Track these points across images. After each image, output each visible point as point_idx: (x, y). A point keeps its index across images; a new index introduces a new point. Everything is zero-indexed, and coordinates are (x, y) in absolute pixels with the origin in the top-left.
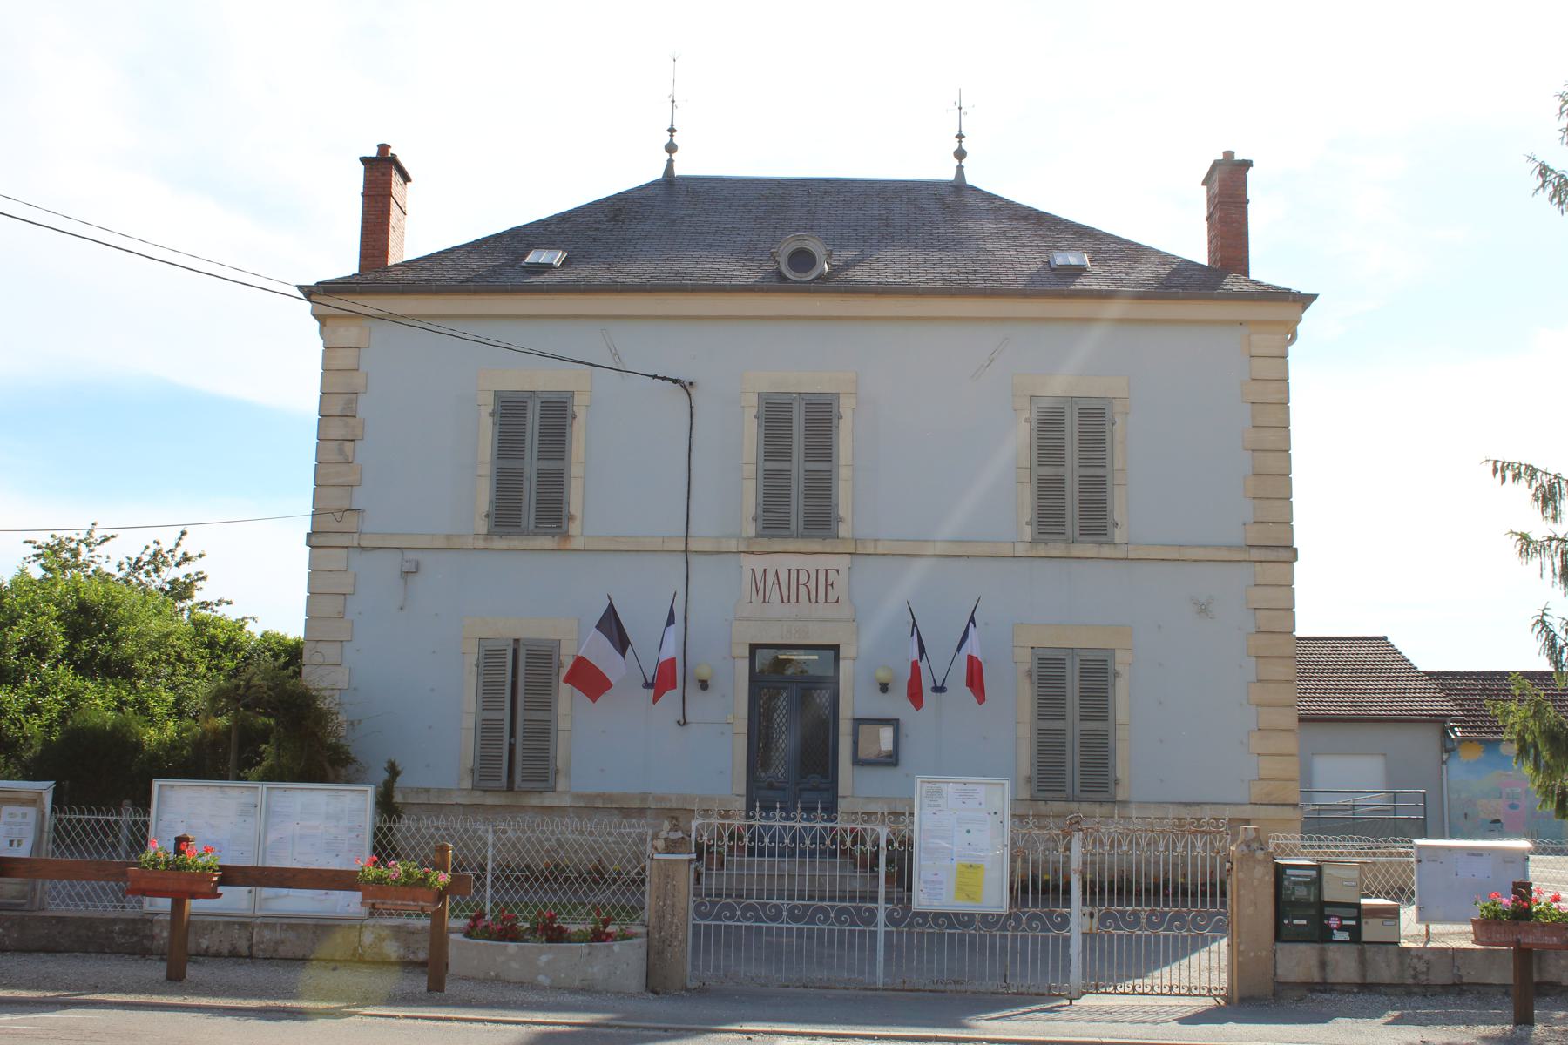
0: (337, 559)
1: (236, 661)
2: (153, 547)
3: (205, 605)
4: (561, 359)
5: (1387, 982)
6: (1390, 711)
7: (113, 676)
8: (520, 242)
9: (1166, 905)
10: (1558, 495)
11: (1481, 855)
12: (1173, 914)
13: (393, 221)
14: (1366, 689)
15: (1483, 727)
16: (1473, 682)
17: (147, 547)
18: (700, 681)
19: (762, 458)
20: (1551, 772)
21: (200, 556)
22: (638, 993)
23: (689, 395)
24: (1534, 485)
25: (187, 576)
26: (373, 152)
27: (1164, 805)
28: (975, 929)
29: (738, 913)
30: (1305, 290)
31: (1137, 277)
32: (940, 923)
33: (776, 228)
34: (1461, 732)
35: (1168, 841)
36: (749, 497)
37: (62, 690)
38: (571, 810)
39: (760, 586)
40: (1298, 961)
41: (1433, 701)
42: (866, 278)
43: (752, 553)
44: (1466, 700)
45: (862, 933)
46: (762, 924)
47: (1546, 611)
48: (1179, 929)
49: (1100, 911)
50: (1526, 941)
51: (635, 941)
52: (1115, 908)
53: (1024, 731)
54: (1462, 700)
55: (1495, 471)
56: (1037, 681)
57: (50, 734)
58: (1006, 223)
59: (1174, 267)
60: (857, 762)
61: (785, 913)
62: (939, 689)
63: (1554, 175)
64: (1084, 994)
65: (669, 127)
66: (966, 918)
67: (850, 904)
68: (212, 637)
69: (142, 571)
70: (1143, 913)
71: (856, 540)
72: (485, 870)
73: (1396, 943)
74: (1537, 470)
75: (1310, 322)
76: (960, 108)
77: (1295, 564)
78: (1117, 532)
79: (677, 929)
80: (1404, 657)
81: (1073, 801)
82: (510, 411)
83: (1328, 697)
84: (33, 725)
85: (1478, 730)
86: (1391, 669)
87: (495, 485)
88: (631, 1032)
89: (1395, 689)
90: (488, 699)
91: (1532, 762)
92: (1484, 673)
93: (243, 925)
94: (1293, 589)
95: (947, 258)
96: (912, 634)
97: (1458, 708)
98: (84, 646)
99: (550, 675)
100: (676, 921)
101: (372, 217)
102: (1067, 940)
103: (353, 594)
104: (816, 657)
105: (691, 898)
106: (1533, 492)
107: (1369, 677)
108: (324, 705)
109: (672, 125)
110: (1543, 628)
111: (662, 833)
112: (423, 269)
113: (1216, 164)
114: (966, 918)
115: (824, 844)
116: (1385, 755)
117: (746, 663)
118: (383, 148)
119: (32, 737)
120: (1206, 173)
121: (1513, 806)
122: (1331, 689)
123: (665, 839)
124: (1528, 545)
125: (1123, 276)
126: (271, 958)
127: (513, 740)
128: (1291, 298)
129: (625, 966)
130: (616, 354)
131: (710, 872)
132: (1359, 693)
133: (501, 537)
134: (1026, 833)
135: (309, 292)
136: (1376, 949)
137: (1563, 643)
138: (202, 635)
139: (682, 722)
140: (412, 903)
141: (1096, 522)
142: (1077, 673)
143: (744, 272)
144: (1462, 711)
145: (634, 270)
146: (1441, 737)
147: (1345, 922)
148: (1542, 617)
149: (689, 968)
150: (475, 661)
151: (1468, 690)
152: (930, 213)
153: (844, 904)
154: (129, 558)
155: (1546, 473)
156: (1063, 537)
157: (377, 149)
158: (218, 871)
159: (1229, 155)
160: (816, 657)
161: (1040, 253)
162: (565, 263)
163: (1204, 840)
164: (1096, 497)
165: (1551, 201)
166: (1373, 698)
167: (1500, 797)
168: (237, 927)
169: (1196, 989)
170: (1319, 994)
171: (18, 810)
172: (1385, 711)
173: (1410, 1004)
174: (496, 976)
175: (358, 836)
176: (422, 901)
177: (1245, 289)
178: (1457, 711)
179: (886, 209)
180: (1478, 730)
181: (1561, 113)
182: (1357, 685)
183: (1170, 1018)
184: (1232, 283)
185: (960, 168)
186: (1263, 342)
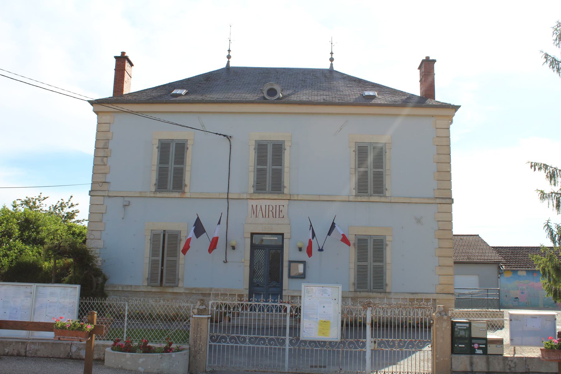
0: (100, 200)
1: (82, 240)
2: (61, 201)
3: (78, 221)
4: (180, 125)
7: (37, 244)
8: (171, 87)
9: (406, 338)
11: (536, 318)
12: (409, 342)
13: (126, 79)
14: (472, 252)
15: (512, 266)
16: (508, 250)
17: (59, 202)
18: (232, 246)
19: (256, 164)
20: (555, 282)
21: (77, 204)
23: (230, 141)
25: (73, 211)
26: (119, 55)
27: (404, 294)
28: (326, 348)
29: (228, 340)
30: (456, 104)
31: (395, 100)
33: (264, 83)
34: (505, 267)
35: (407, 311)
36: (251, 178)
38: (184, 294)
41: (495, 257)
42: (295, 99)
43: (252, 199)
44: (506, 256)
45: (279, 349)
46: (238, 345)
47: (549, 221)
49: (378, 340)
52: (385, 339)
53: (352, 266)
54: (505, 256)
55: (532, 166)
57: (12, 264)
58: (348, 82)
59: (408, 96)
60: (290, 277)
63: (550, 58)
66: (323, 343)
67: (274, 337)
69: (57, 209)
70: (396, 341)
73: (502, 355)
74: (548, 166)
76: (332, 44)
77: (453, 204)
79: (202, 347)
80: (484, 242)
81: (370, 292)
82: (164, 147)
83: (459, 255)
85: (510, 266)
86: (480, 246)
89: (482, 252)
90: (154, 252)
93: (23, 343)
94: (452, 214)
96: (310, 229)
97: (503, 259)
98: (26, 233)
99: (177, 243)
100: (201, 343)
101: (118, 77)
102: (365, 352)
103: (105, 213)
104: (277, 238)
105: (208, 333)
106: (546, 174)
107: (473, 248)
108: (92, 254)
109: (229, 49)
110: (548, 228)
112: (135, 95)
113: (423, 61)
114: (323, 343)
116: (479, 275)
118: (123, 53)
119: (5, 265)
121: (522, 293)
122: (460, 252)
123: (198, 309)
124: (544, 195)
125: (389, 99)
126: (34, 357)
128: (451, 107)
131: (234, 318)
132: (470, 254)
135: (92, 103)
136: (493, 357)
137: (556, 233)
138: (70, 231)
139: (225, 262)
140: (76, 338)
142: (372, 245)
144: (505, 260)
145: (211, 96)
146: (498, 269)
147: (481, 346)
148: (547, 223)
149: (207, 363)
150: (149, 238)
151: (507, 253)
152: (320, 79)
153: (272, 337)
154: (53, 205)
155: (551, 167)
156: (367, 194)
157: (121, 53)
159: (428, 58)
160: (277, 238)
161: (359, 91)
162: (186, 94)
163: (422, 311)
166: (475, 255)
167: (518, 290)
168: (20, 343)
172: (479, 260)
175: (73, 306)
176: (80, 337)
177: (434, 104)
178: (503, 260)
179: (304, 77)
180: (510, 266)
181: (553, 34)
182: (469, 251)
184: (429, 102)
185: (332, 64)
186: (441, 123)
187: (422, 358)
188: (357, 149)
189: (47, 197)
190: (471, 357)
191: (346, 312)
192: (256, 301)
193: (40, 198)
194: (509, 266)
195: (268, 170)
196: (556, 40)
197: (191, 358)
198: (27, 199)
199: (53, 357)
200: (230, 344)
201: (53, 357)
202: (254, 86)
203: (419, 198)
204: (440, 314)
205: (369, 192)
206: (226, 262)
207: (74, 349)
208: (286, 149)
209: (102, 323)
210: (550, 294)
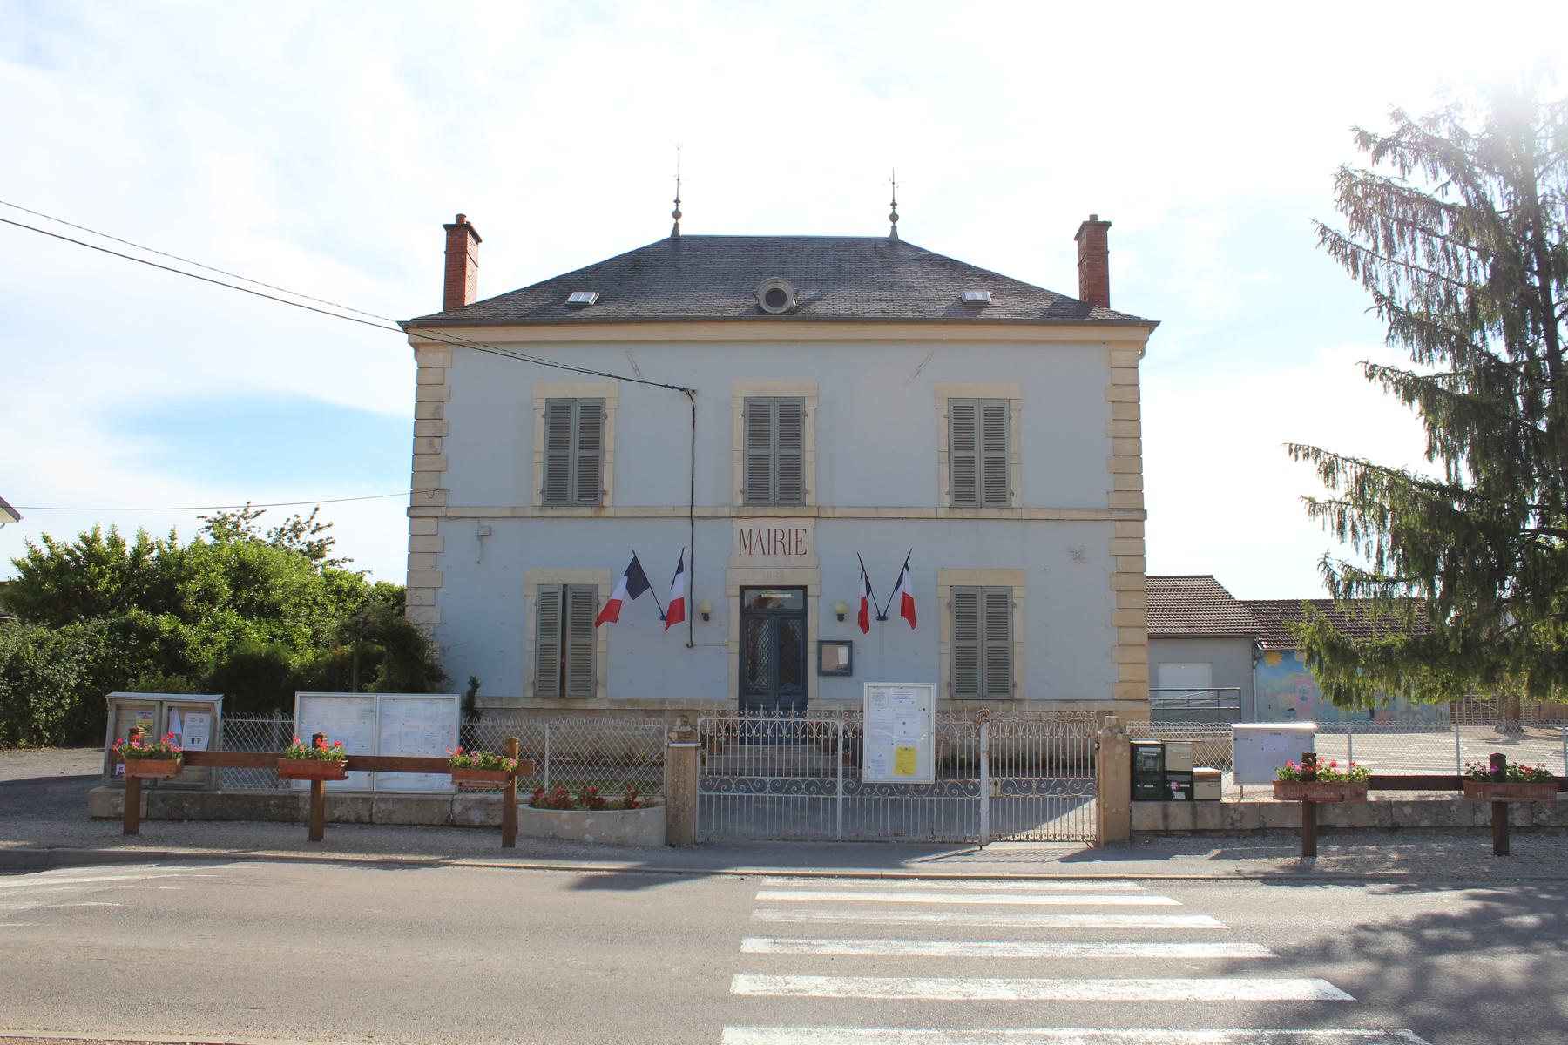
0: (429, 526)
3: (333, 562)
7: (266, 616)
9: (1051, 775)
11: (1280, 734)
13: (468, 272)
17: (288, 520)
21: (329, 526)
23: (692, 400)
24: (1319, 461)
25: (320, 541)
29: (733, 786)
38: (608, 711)
39: (746, 543)
40: (1148, 815)
42: (824, 311)
45: (826, 800)
48: (1061, 792)
49: (1002, 780)
51: (657, 808)
52: (1014, 778)
53: (946, 648)
55: (1291, 451)
57: (220, 660)
58: (929, 268)
60: (821, 673)
61: (768, 786)
62: (882, 618)
63: (1331, 234)
64: (990, 842)
65: (675, 199)
66: (903, 788)
68: (339, 586)
69: (286, 538)
71: (819, 508)
73: (1219, 800)
74: (1320, 451)
75: (1154, 341)
77: (1145, 522)
78: (1013, 498)
82: (557, 413)
84: (208, 653)
88: (654, 875)
90: (545, 630)
92: (1283, 601)
93: (365, 800)
95: (884, 295)
96: (862, 577)
98: (244, 594)
100: (686, 792)
102: (978, 803)
104: (790, 595)
108: (422, 636)
113: (1084, 225)
115: (797, 735)
117: (737, 600)
118: (461, 217)
121: (1303, 699)
123: (678, 732)
124: (1315, 507)
125: (1016, 307)
126: (387, 824)
128: (1140, 324)
135: (406, 326)
137: (1339, 578)
141: (998, 491)
142: (985, 605)
143: (732, 306)
145: (650, 306)
147: (1182, 786)
153: (812, 778)
154: (276, 529)
156: (973, 503)
159: (1094, 217)
160: (790, 595)
162: (598, 302)
165: (1329, 253)
167: (1294, 692)
168: (360, 801)
171: (198, 716)
177: (1107, 317)
183: (1054, 858)
184: (1097, 312)
185: (894, 228)
186: (1120, 357)
187: (1079, 818)
188: (952, 411)
190: (1166, 805)
191: (943, 732)
192: (782, 716)
193: (247, 513)
194: (1276, 641)
195: (772, 459)
196: (1341, 200)
197: (669, 818)
198: (219, 517)
199: (420, 824)
200: (738, 794)
201: (420, 824)
202: (734, 281)
203: (1079, 509)
204: (1111, 731)
207: (457, 809)
208: (806, 415)
210: (1329, 695)
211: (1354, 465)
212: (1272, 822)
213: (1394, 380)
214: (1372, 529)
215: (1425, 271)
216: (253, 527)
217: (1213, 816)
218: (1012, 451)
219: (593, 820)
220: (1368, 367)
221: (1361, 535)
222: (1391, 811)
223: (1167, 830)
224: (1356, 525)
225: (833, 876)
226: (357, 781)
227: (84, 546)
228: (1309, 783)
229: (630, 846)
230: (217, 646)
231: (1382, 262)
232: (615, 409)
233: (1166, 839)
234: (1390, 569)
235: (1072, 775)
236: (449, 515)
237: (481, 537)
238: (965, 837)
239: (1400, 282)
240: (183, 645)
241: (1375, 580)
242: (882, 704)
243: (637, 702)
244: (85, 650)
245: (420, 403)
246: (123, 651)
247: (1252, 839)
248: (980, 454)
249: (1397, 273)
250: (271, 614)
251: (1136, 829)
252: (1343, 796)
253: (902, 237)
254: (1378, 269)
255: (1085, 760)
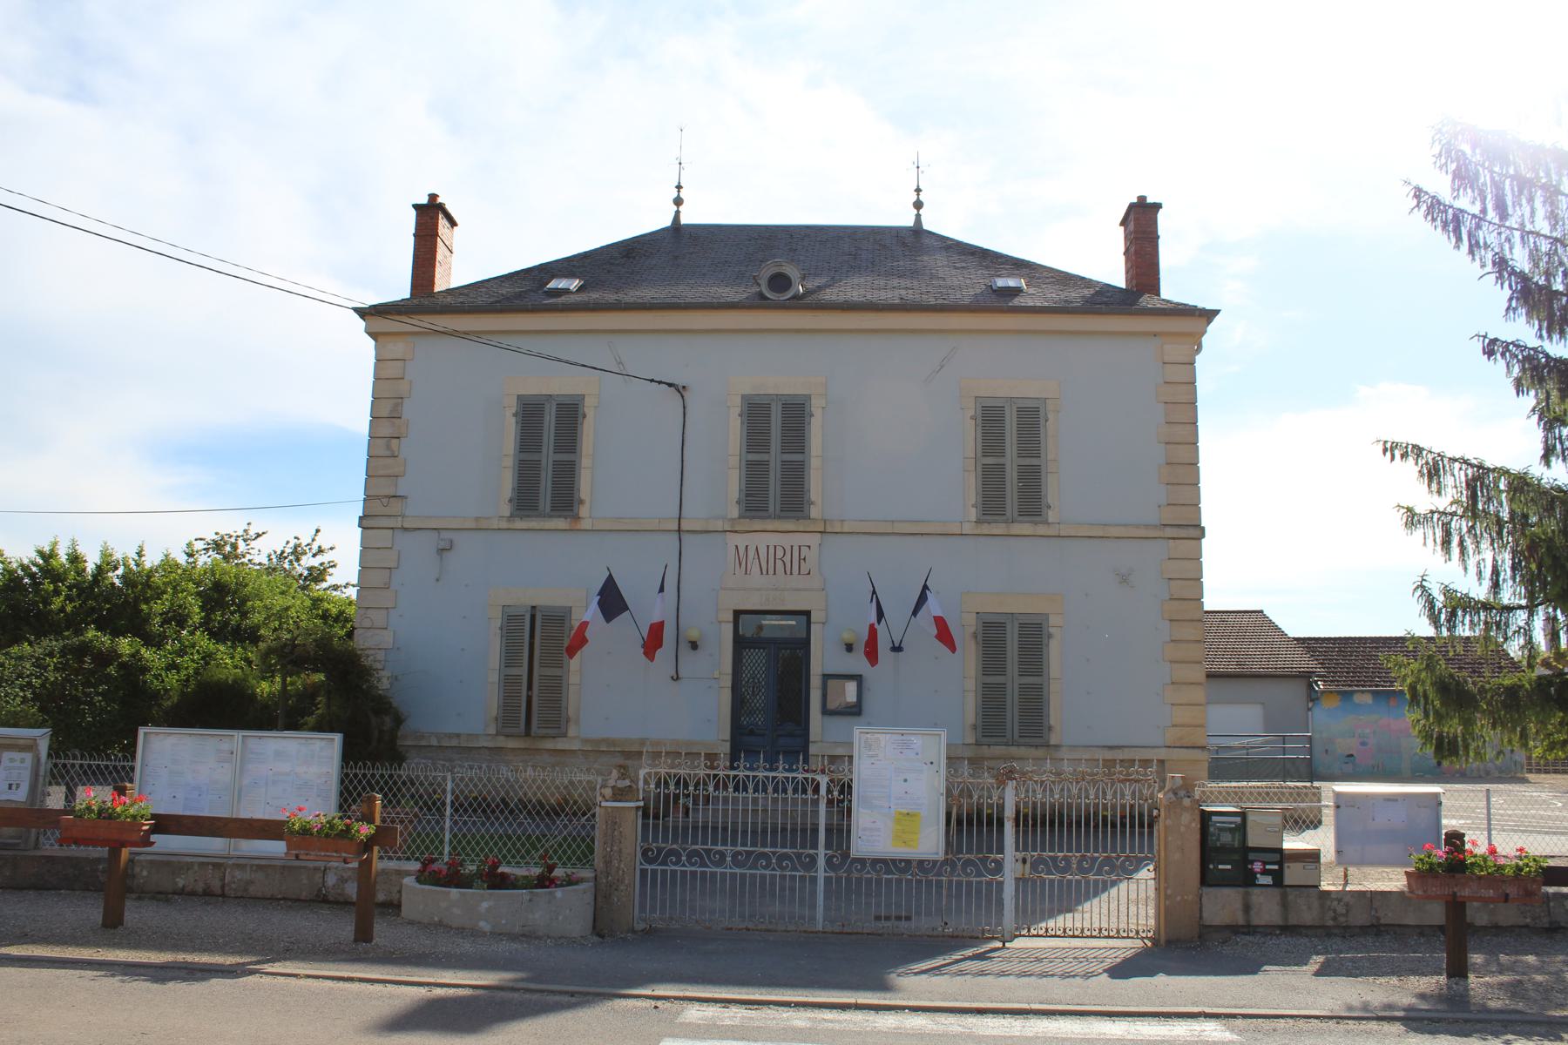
0: (383, 538)
2: (293, 542)
3: (335, 588)
4: (567, 362)
5: (1308, 924)
6: (1267, 668)
7: (242, 641)
9: (1096, 850)
10: (1442, 471)
12: (1103, 860)
13: (439, 257)
15: (1340, 681)
17: (288, 542)
19: (744, 450)
21: (332, 549)
22: (582, 937)
23: (682, 397)
24: (1420, 462)
25: (322, 564)
28: (911, 875)
29: (684, 858)
32: (878, 868)
35: (1098, 789)
36: (733, 485)
37: (198, 651)
39: (741, 561)
40: (1223, 905)
42: (834, 298)
43: (736, 532)
45: (802, 878)
48: (1108, 873)
49: (1032, 856)
50: (1463, 894)
51: (581, 887)
53: (970, 684)
54: (1323, 660)
55: (1385, 450)
56: (981, 642)
58: (956, 257)
59: (1097, 289)
60: (826, 712)
61: (729, 859)
62: (897, 649)
63: (1427, 197)
64: (1017, 936)
65: (677, 184)
66: (903, 864)
69: (287, 560)
70: (1073, 858)
71: (825, 521)
72: (445, 816)
73: (1316, 887)
74: (1423, 449)
75: (1213, 335)
76: (918, 167)
77: (1203, 540)
78: (1050, 513)
79: (623, 874)
82: (530, 412)
84: (172, 679)
87: (517, 475)
88: (535, 997)
90: (509, 658)
91: (1423, 710)
92: (1340, 638)
93: (216, 866)
95: (903, 282)
98: (218, 616)
100: (622, 866)
102: (1001, 885)
104: (794, 623)
108: (366, 662)
110: (1423, 592)
111: (610, 781)
112: (461, 294)
113: (1132, 206)
116: (1263, 704)
117: (730, 627)
118: (433, 197)
120: (1123, 215)
121: (1363, 744)
123: (613, 787)
124: (1413, 518)
125: (1054, 295)
126: (242, 897)
127: (530, 693)
128: (1197, 313)
129: (568, 911)
130: (621, 363)
133: (521, 518)
134: (961, 782)
135: (362, 313)
136: (1298, 893)
139: (675, 678)
140: (335, 854)
141: (1032, 505)
144: (1324, 668)
145: (638, 293)
147: (1268, 867)
153: (785, 850)
155: (1431, 452)
156: (1004, 517)
157: (427, 198)
158: (149, 820)
159: (1142, 199)
160: (794, 623)
162: (580, 289)
163: (1132, 787)
164: (1032, 482)
165: (1426, 218)
167: (1354, 736)
168: (210, 867)
169: (1124, 931)
170: (1243, 937)
171: (17, 755)
173: (1331, 945)
174: (440, 921)
176: (345, 852)
177: (1158, 306)
179: (856, 247)
183: (1099, 968)
184: (1146, 301)
185: (918, 216)
186: (1174, 351)
189: (263, 533)
191: (956, 793)
194: (1360, 681)
195: (772, 464)
196: (1440, 155)
201: (284, 899)
202: (736, 270)
204: (1175, 794)
205: (1009, 513)
206: (678, 678)
209: (393, 822)
211: (1464, 466)
212: (1388, 917)
213: (1520, 357)
214: (1485, 544)
215: (1546, 237)
216: (252, 548)
217: (1309, 908)
218: (1049, 458)
219: (492, 903)
220: (1487, 341)
221: (1471, 552)
222: (1548, 906)
223: (1249, 926)
224: (1498, 534)
225: (787, 1004)
226: (165, 843)
227: (41, 562)
228: (1458, 876)
229: (539, 938)
230: (184, 672)
231: (1491, 228)
232: (596, 407)
233: (1248, 938)
234: (1510, 594)
235: (1123, 850)
236: (405, 526)
237: (441, 551)
238: (983, 930)
239: (1514, 251)
240: (145, 670)
241: (1486, 606)
242: (877, 755)
243: (612, 742)
244: (31, 674)
245: (376, 399)
246: (76, 676)
247: (1362, 939)
248: (1011, 460)
249: (1510, 241)
250: (248, 638)
251: (1208, 923)
252: (1507, 895)
253: (927, 226)
254: (1487, 236)
255: (1132, 817)
